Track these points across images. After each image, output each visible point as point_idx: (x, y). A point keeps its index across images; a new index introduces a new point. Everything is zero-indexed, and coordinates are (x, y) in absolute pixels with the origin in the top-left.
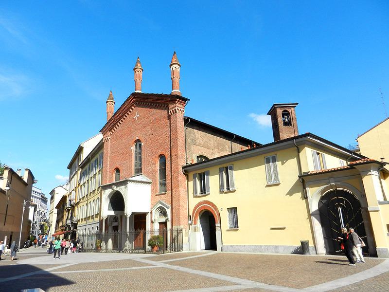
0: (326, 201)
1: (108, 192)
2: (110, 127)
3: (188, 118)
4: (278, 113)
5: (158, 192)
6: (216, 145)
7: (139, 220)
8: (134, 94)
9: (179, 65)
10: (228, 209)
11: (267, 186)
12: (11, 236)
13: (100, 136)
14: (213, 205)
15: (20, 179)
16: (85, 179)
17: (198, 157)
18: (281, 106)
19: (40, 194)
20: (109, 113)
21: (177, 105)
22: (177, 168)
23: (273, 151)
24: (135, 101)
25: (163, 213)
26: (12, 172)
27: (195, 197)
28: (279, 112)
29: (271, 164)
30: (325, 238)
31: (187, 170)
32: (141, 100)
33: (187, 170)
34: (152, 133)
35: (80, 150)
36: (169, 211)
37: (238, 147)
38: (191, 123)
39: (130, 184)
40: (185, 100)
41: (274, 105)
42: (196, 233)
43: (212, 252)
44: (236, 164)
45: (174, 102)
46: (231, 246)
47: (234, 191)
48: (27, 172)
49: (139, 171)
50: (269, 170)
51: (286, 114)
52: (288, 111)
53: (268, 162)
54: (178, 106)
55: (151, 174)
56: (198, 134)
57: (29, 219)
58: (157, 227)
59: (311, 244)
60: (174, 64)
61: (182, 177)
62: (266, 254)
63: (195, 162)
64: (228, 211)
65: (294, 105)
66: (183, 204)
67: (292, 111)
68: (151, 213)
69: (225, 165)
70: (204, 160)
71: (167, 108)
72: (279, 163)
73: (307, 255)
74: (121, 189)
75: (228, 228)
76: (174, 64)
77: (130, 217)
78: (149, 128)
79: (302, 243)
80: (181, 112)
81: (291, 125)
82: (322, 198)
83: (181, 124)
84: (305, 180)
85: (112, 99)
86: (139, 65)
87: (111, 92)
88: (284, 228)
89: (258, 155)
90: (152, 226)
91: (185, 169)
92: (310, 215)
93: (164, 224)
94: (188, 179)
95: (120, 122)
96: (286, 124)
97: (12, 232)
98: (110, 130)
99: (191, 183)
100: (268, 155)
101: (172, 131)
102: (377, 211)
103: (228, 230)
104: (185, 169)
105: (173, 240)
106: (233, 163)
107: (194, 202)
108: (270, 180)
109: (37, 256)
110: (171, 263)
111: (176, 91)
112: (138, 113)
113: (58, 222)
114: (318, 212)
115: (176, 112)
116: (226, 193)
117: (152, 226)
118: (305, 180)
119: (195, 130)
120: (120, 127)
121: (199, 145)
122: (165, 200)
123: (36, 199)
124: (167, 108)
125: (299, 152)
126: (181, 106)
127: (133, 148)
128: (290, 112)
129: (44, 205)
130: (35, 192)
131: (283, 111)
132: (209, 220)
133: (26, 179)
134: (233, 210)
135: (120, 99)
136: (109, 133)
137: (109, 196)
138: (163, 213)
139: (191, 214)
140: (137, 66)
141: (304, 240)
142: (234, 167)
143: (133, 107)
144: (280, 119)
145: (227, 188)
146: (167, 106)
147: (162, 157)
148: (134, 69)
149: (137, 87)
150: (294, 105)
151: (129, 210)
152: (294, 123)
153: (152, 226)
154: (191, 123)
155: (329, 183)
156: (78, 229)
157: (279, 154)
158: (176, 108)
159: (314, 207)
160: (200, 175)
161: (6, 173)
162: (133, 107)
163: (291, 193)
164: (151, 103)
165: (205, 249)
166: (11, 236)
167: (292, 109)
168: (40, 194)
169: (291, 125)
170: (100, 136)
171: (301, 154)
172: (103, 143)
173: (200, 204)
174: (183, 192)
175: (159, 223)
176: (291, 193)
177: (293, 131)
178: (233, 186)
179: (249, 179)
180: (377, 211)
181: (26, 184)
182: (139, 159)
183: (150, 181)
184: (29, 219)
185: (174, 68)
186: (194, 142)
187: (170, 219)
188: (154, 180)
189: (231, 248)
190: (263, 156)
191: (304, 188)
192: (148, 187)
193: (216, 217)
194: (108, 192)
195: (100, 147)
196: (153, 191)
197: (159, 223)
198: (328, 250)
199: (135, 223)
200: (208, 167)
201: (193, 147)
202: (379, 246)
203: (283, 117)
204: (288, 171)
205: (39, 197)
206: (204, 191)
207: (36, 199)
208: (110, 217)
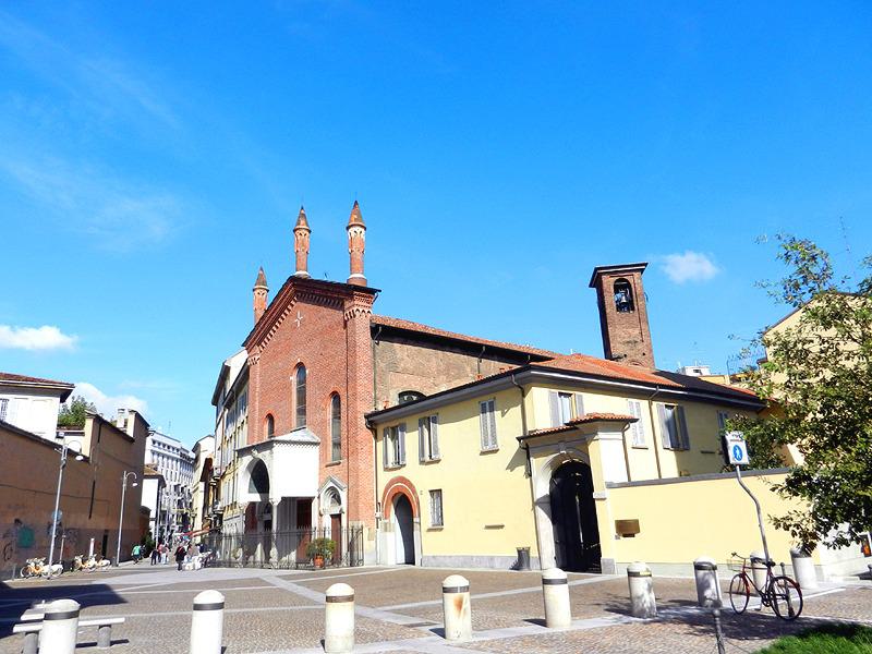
0: (559, 480)
1: (247, 459)
2: (255, 340)
3: (378, 325)
4: (605, 286)
5: (330, 461)
6: (443, 367)
7: (300, 509)
8: (292, 279)
9: (362, 226)
10: (431, 491)
11: (483, 453)
12: (105, 537)
13: (243, 355)
14: (411, 485)
15: (121, 434)
16: (232, 429)
17: (401, 395)
18: (612, 270)
19: (178, 450)
20: (258, 311)
21: (356, 302)
22: (356, 418)
23: (488, 394)
24: (296, 292)
25: (337, 499)
26: (99, 420)
27: (386, 469)
28: (608, 282)
29: (488, 413)
30: (556, 543)
31: (373, 421)
32: (305, 289)
33: (373, 421)
34: (321, 351)
35: (226, 371)
36: (343, 495)
37: (493, 367)
38: (383, 333)
39: (277, 448)
40: (372, 292)
41: (596, 269)
42: (388, 533)
43: (411, 566)
44: (442, 412)
45: (351, 297)
46: (434, 557)
47: (438, 461)
48: (132, 419)
49: (302, 426)
50: (485, 420)
51: (622, 286)
52: (626, 280)
53: (484, 412)
54: (357, 304)
55: (319, 428)
56: (402, 351)
57: (144, 503)
58: (327, 522)
59: (534, 554)
60: (352, 226)
61: (364, 433)
62: (479, 570)
63: (394, 402)
64: (432, 496)
65: (640, 268)
66: (366, 483)
67: (634, 279)
68: (319, 497)
69: (393, 424)
70: (415, 398)
71: (342, 308)
72: (498, 414)
73: (525, 571)
74: (264, 456)
75: (430, 526)
76: (352, 226)
77: (278, 506)
78: (317, 342)
79: (519, 552)
80: (363, 315)
81: (633, 309)
82: (554, 476)
83: (363, 336)
84: (530, 444)
85: (264, 283)
86: (302, 222)
87: (262, 269)
88: (502, 527)
89: (461, 401)
90: (320, 521)
91: (371, 419)
92: (536, 503)
93: (337, 517)
94: (376, 437)
95: (274, 328)
96: (620, 307)
97: (106, 531)
98: (259, 344)
99: (380, 444)
100: (487, 399)
101: (350, 348)
102: (604, 499)
103: (429, 530)
104: (371, 419)
105: (351, 547)
106: (437, 411)
107: (385, 478)
108: (486, 444)
109: (132, 573)
110: (299, 584)
111: (356, 277)
112: (302, 313)
113: (205, 506)
114: (548, 500)
115: (355, 316)
116: (429, 463)
117: (320, 521)
118: (530, 444)
119: (395, 344)
120: (275, 337)
121: (405, 371)
122: (337, 475)
123: (165, 459)
124: (342, 308)
125: (524, 396)
126: (365, 304)
127: (294, 378)
128: (631, 282)
129: (189, 473)
130: (169, 447)
131: (617, 281)
132: (404, 506)
133: (130, 432)
134: (437, 493)
135: (276, 284)
136: (257, 349)
137: (248, 467)
138: (337, 499)
139: (380, 501)
140: (299, 224)
141: (522, 546)
142: (440, 418)
143: (293, 302)
144: (611, 299)
145: (429, 458)
146: (343, 304)
147: (335, 396)
148: (295, 231)
149: (300, 265)
150: (640, 268)
151: (275, 497)
152: (639, 303)
153: (321, 522)
154: (383, 333)
155: (558, 451)
156: (224, 523)
157: (499, 397)
158: (355, 309)
159: (543, 488)
160: (393, 428)
161: (89, 424)
162: (293, 302)
163: (511, 467)
164: (320, 296)
165: (407, 563)
166: (105, 537)
167: (636, 274)
168: (178, 450)
169: (633, 309)
170: (243, 355)
171: (527, 399)
172: (249, 367)
173: (392, 482)
174: (363, 464)
175: (332, 516)
176: (511, 467)
177: (636, 322)
178: (437, 452)
179: (457, 435)
180: (604, 499)
181: (131, 440)
182: (302, 399)
183: (317, 439)
184: (144, 503)
185: (353, 234)
186: (393, 367)
187: (345, 510)
188: (324, 438)
189: (433, 561)
190: (477, 400)
191: (529, 458)
192: (315, 450)
193: (414, 505)
194: (247, 459)
195: (245, 373)
196: (322, 456)
197: (332, 516)
198: (560, 563)
199: (298, 514)
200: (404, 417)
201: (391, 376)
202: (605, 556)
203: (616, 292)
204: (508, 425)
205: (175, 456)
206: (399, 464)
207: (170, 461)
208: (252, 505)
